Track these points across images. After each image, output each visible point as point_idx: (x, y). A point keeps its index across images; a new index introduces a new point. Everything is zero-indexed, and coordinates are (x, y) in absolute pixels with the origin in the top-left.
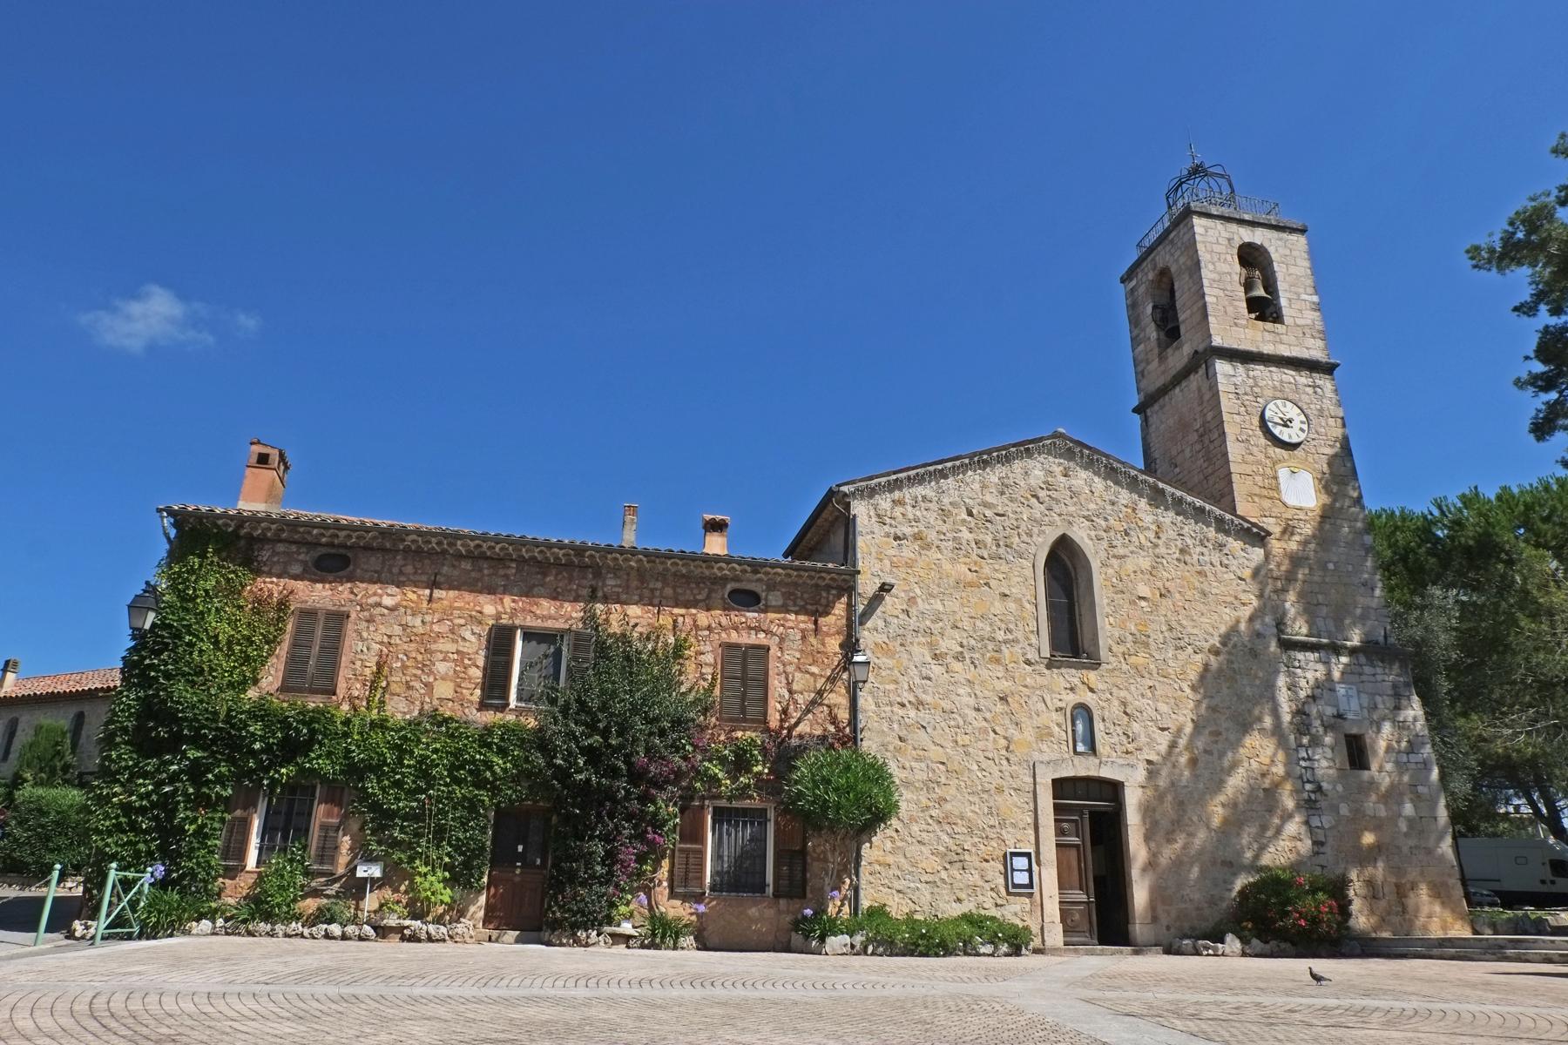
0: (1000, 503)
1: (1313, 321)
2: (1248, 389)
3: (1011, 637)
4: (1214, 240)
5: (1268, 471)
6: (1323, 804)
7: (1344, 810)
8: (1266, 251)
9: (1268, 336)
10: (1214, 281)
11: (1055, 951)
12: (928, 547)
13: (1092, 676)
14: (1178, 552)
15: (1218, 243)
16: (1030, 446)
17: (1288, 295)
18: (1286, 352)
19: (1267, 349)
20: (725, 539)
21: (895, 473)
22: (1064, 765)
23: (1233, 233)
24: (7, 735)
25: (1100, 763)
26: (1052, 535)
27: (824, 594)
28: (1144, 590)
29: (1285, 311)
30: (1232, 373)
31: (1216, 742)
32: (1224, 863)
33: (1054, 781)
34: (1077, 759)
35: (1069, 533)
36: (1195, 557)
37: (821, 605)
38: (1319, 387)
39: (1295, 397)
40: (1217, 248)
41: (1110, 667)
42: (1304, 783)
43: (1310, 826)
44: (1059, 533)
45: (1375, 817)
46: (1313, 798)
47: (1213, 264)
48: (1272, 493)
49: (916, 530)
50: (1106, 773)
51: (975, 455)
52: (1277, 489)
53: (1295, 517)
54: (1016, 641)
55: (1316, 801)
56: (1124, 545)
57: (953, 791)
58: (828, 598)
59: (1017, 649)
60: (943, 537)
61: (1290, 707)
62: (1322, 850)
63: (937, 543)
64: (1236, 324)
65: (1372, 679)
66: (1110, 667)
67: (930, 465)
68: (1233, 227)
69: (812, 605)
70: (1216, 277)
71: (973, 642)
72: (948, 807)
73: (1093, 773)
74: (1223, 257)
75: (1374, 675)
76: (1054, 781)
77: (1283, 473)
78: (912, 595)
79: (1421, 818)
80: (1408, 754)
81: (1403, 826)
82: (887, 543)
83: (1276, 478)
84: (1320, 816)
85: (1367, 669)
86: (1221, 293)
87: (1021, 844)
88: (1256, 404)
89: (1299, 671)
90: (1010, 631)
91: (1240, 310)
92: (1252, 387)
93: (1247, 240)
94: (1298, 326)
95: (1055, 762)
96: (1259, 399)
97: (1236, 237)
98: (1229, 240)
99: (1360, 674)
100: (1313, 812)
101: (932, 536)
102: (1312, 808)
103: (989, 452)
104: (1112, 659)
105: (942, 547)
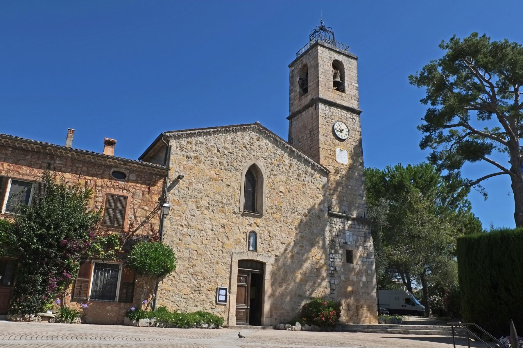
1: (355, 94)
3: (229, 202)
6: (336, 275)
7: (343, 278)
12: (200, 162)
13: (259, 221)
16: (246, 127)
18: (344, 104)
19: (338, 102)
21: (190, 130)
26: (250, 163)
27: (154, 177)
28: (282, 189)
29: (346, 88)
31: (301, 250)
37: (152, 181)
38: (354, 119)
39: (345, 122)
49: (196, 155)
50: (259, 259)
51: (223, 127)
52: (335, 156)
54: (231, 204)
55: (334, 274)
56: (277, 171)
57: (199, 262)
58: (155, 179)
64: (328, 91)
65: (358, 230)
66: (266, 218)
67: (205, 129)
68: (332, 53)
69: (148, 181)
71: (213, 203)
72: (196, 268)
73: (254, 259)
76: (239, 261)
77: (338, 150)
78: (191, 181)
81: (361, 285)
82: (183, 159)
83: (335, 151)
85: (357, 227)
86: (325, 78)
87: (224, 285)
89: (334, 225)
91: (331, 85)
92: (331, 116)
93: (336, 59)
96: (333, 121)
98: (330, 57)
99: (354, 228)
101: (202, 158)
102: (332, 277)
103: (229, 127)
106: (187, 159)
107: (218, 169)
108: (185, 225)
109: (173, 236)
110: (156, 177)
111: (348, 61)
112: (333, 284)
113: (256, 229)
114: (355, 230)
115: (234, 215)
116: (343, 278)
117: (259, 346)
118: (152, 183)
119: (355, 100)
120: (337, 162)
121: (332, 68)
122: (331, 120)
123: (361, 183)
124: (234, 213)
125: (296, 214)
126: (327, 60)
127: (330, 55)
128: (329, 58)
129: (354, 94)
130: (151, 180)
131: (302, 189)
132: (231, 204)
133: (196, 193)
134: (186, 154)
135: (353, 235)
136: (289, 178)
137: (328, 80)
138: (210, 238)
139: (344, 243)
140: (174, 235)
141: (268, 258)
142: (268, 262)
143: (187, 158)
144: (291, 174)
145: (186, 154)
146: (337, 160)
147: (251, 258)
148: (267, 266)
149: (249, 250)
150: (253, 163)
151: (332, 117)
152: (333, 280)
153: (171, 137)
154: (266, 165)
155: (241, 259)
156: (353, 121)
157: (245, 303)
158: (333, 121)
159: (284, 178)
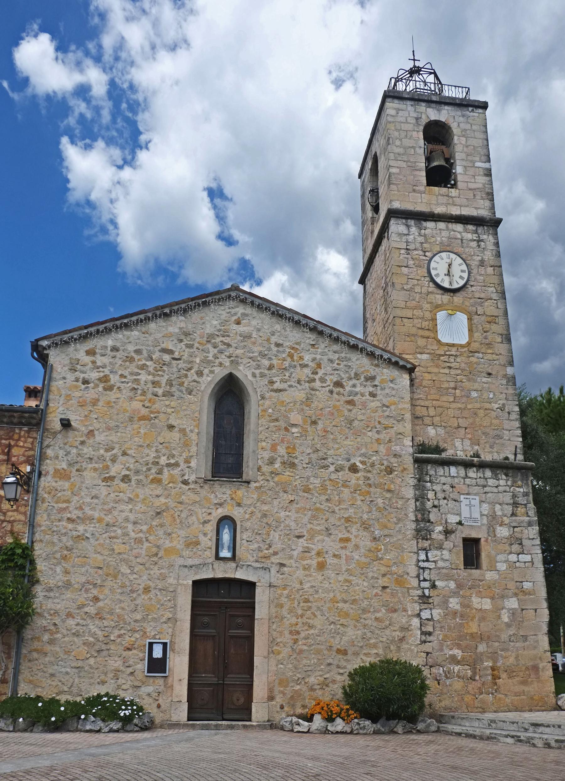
0: (178, 349)
1: (484, 184)
2: (418, 245)
3: (172, 461)
4: (403, 120)
5: (428, 315)
6: (436, 600)
7: (454, 603)
8: (450, 128)
9: (444, 200)
10: (399, 154)
11: (176, 725)
12: (111, 388)
13: (241, 492)
14: (332, 384)
15: (407, 122)
16: (207, 299)
17: (464, 163)
18: (455, 211)
19: (439, 210)
20: (45, 38)
21: (86, 327)
22: (204, 569)
23: (421, 113)
24: (462, 108)
25: (237, 567)
26: (220, 373)
27: (17, 431)
28: (295, 418)
29: (459, 178)
30: (406, 232)
31: (345, 548)
32: (339, 651)
33: (194, 582)
34: (217, 564)
35: (235, 372)
36: (348, 388)
37: (13, 440)
38: (482, 241)
39: (460, 250)
40: (405, 127)
41: (257, 484)
42: (420, 581)
43: (421, 618)
44: (226, 372)
45: (481, 609)
46: (427, 594)
47: (401, 140)
48: (427, 333)
49: (102, 374)
50: (240, 575)
51: (157, 308)
52: (434, 329)
53: (447, 353)
54: (177, 465)
55: (429, 597)
56: (282, 381)
57: (107, 591)
58: (20, 433)
59: (176, 472)
60: (124, 380)
61: (416, 516)
62: (429, 638)
63: (118, 384)
64: (414, 191)
65: (495, 490)
66: (257, 484)
67: (117, 319)
68: (422, 107)
69: (6, 439)
70: (401, 150)
71: (139, 467)
72: (100, 604)
73: (230, 575)
74: (409, 134)
75: (497, 487)
76: (194, 582)
77: (441, 315)
78: (91, 428)
79: (523, 610)
80: (518, 554)
81: (505, 618)
82: (76, 387)
83: (434, 320)
84: (431, 609)
85: (491, 482)
86: (404, 165)
87: (161, 636)
88: (424, 258)
89: (429, 484)
90: (173, 456)
91: (420, 178)
92: (422, 243)
93: (433, 118)
94: (470, 189)
95: (197, 566)
96: (427, 254)
97: (424, 116)
98: (417, 119)
99: (484, 486)
100: (426, 606)
101: (114, 379)
102: (424, 603)
103: (170, 305)
104: (260, 478)
105: (122, 388)
106: (83, 387)
107: (149, 396)
108: (78, 517)
109: (53, 543)
110: (21, 429)
111: (463, 116)
112: (428, 619)
113: (237, 513)
114: (486, 489)
115: (184, 486)
116: (454, 603)
117: (108, 779)
118: (12, 443)
119: (482, 198)
120: (439, 341)
121: (422, 142)
122: (421, 253)
123: (504, 382)
124: (185, 482)
125: (332, 468)
126: (410, 127)
127: (415, 115)
128: (414, 121)
129: (480, 186)
130: (11, 438)
131: (346, 413)
132: (177, 465)
133: (102, 452)
134: (82, 375)
135: (481, 502)
136: (313, 392)
137: (414, 168)
138: (130, 539)
139: (457, 523)
140: (55, 541)
141: (261, 572)
142: (262, 580)
143: (84, 384)
144: (317, 384)
145: (82, 375)
146: (440, 337)
147: (220, 575)
148: (258, 591)
149: (217, 558)
150: (227, 372)
151: (425, 245)
152: (428, 611)
153: (49, 347)
154: (257, 372)
155: (198, 577)
156: (479, 246)
157: (214, 674)
158: (427, 254)
159: (299, 394)
